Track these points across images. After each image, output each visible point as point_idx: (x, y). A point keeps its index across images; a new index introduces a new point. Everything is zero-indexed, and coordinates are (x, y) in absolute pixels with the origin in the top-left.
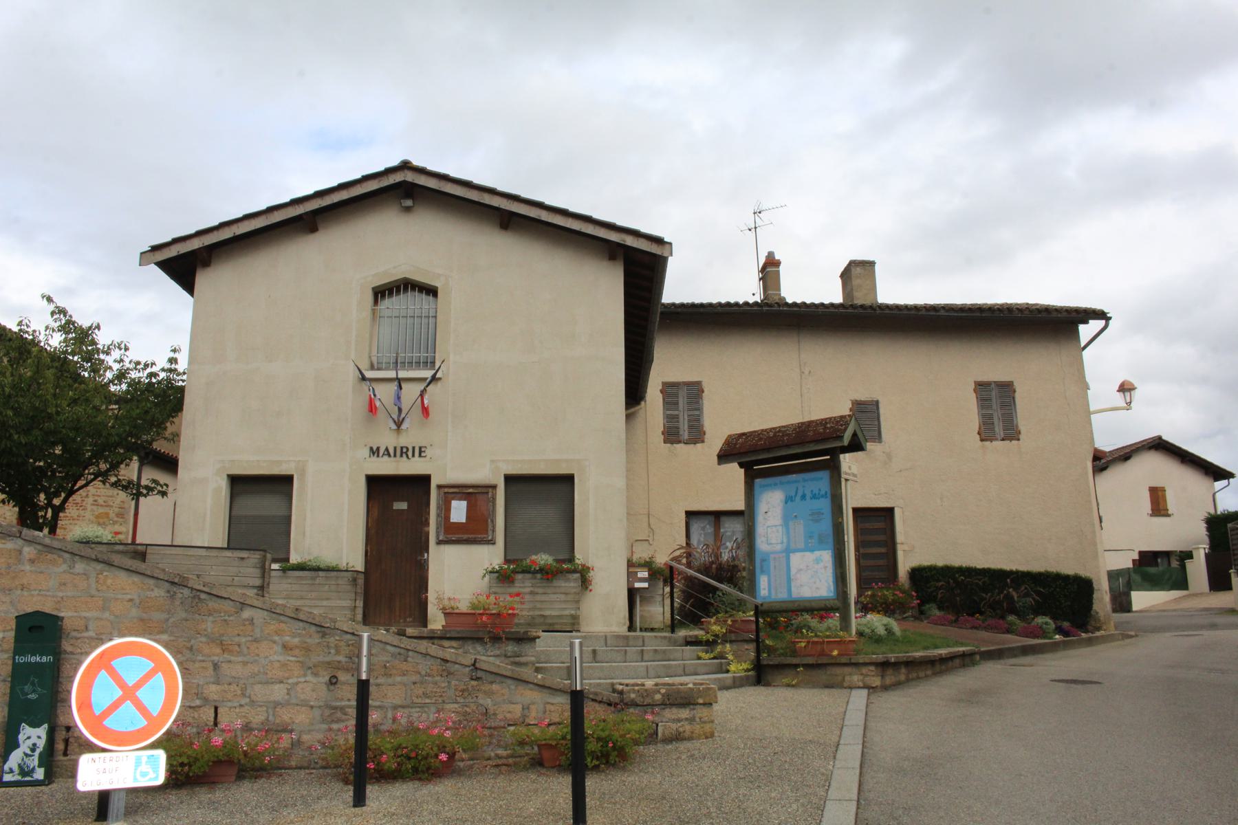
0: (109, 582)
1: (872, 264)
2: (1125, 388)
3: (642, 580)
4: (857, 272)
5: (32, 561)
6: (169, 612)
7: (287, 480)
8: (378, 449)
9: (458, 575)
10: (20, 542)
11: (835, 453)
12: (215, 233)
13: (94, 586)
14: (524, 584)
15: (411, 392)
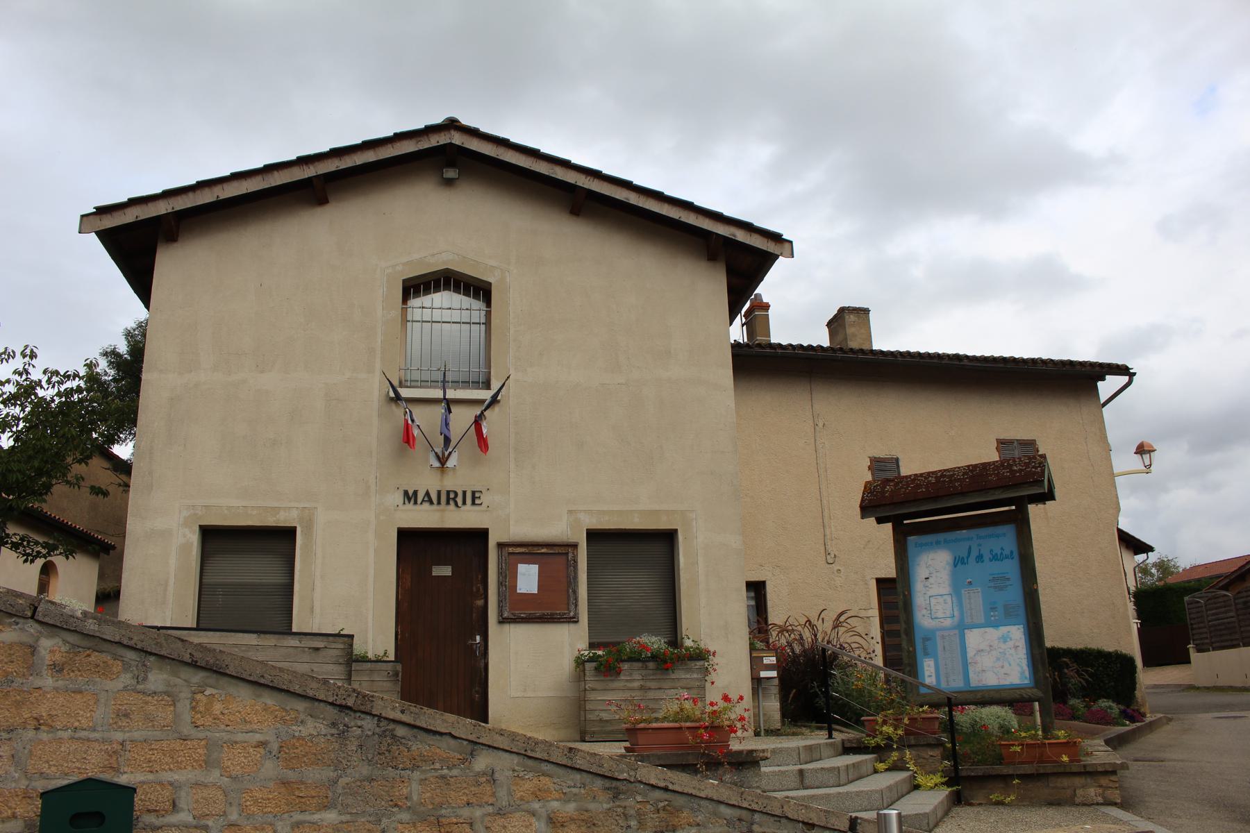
0: (217, 708)
1: (866, 311)
2: (1142, 450)
3: (769, 667)
4: (847, 319)
5: (57, 668)
6: (337, 765)
7: (288, 534)
8: (415, 493)
9: (529, 667)
10: (32, 628)
11: (1021, 504)
12: (191, 195)
13: (187, 717)
14: (632, 677)
15: (462, 418)
